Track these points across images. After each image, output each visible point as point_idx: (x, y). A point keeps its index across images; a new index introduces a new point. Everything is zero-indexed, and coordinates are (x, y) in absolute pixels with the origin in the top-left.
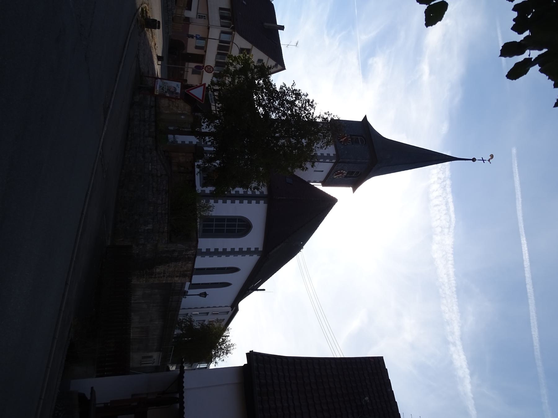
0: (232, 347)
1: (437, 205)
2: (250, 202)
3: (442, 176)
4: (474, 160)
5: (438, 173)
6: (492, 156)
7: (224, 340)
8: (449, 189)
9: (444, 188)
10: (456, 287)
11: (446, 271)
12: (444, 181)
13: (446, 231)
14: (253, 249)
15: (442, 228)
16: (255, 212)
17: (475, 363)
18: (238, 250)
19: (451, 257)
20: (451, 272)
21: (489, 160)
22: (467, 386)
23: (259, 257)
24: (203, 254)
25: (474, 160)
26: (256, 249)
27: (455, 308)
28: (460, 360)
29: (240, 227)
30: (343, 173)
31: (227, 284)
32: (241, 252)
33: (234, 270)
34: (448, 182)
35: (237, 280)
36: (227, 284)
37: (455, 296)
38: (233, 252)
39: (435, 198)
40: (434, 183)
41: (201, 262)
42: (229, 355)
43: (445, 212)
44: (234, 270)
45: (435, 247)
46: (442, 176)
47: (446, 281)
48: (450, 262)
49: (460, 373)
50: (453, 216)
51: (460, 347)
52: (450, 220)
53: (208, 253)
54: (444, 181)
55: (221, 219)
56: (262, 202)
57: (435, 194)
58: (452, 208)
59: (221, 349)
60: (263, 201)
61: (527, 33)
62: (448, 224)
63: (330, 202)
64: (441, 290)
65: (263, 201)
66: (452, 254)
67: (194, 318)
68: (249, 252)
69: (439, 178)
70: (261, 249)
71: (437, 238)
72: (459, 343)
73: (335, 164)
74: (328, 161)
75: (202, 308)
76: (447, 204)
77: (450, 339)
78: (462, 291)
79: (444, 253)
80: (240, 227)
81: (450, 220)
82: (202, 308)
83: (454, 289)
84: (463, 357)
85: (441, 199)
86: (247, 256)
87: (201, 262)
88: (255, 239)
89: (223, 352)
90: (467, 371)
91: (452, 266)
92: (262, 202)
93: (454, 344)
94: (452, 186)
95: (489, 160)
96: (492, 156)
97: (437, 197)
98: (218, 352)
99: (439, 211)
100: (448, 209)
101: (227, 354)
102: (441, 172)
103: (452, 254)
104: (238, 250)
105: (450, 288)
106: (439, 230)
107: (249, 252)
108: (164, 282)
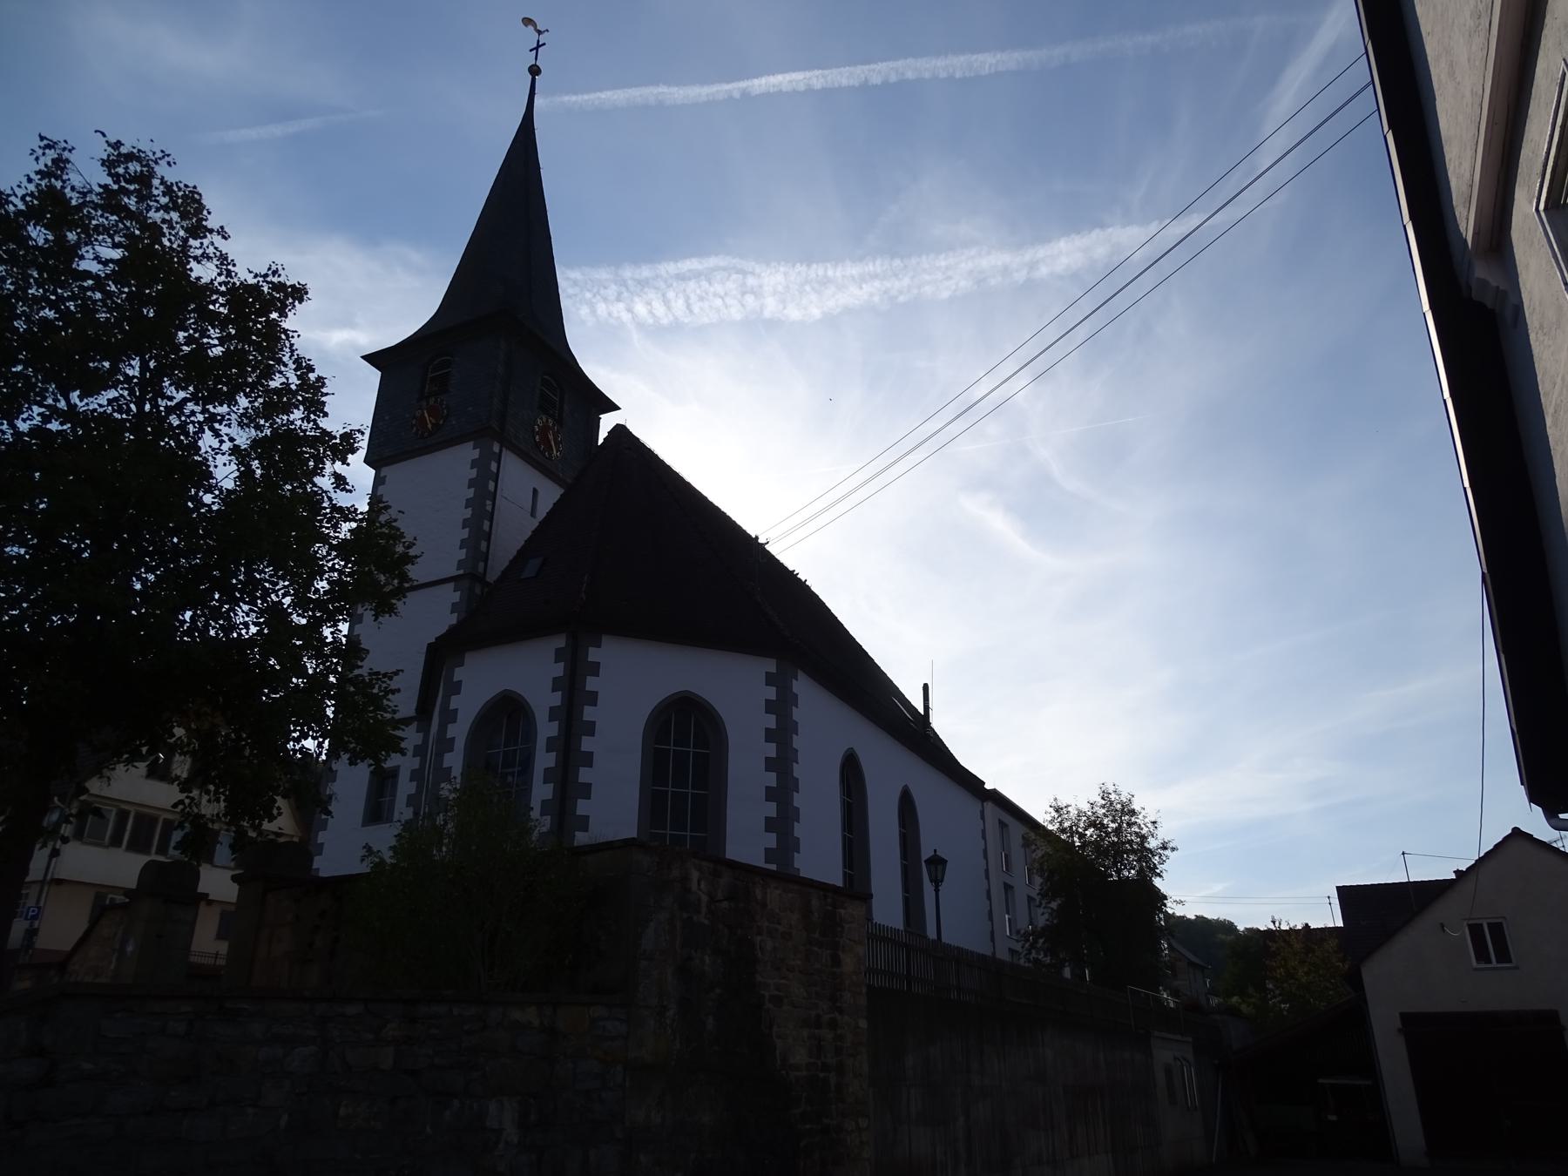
0: (1113, 797)
1: (689, 306)
2: (593, 698)
3: (612, 290)
4: (535, 71)
5: (605, 300)
6: (527, 21)
7: (1092, 824)
8: (645, 272)
9: (643, 284)
10: (892, 258)
11: (852, 285)
12: (624, 283)
13: (751, 281)
14: (771, 692)
15: (744, 294)
16: (633, 680)
17: (1076, 216)
18: (773, 717)
19: (817, 270)
20: (853, 270)
21: (540, 32)
22: (1126, 238)
23: (800, 674)
24: (787, 845)
25: (535, 71)
26: (770, 680)
27: (942, 262)
28: (1067, 254)
29: (684, 741)
30: (544, 430)
31: (907, 804)
32: (782, 734)
33: (851, 770)
34: (628, 273)
35: (888, 771)
36: (907, 804)
37: (914, 261)
38: (782, 763)
39: (669, 308)
40: (630, 310)
41: (820, 860)
42: (1136, 806)
43: (704, 284)
44: (851, 770)
45: (794, 314)
46: (612, 290)
47: (877, 284)
48: (830, 273)
49: (1101, 252)
50: (712, 262)
51: (1041, 252)
52: (724, 269)
53: (783, 823)
54: (624, 283)
55: (653, 804)
56: (593, 655)
57: (659, 309)
58: (691, 264)
59: (1118, 831)
60: (591, 650)
62: (734, 276)
63: (620, 431)
64: (901, 299)
65: (591, 650)
66: (809, 266)
67: (1024, 924)
68: (781, 707)
69: (618, 299)
70: (771, 666)
71: (771, 306)
72: (1028, 255)
73: (507, 444)
74: (494, 466)
75: (989, 897)
76: (681, 277)
77: (1020, 276)
78: (900, 243)
79: (808, 288)
80: (684, 741)
81: (724, 269)
82: (989, 897)
83: (897, 262)
84: (1062, 244)
85: (671, 294)
86: (797, 714)
87: (820, 860)
88: (735, 686)
89: (1130, 824)
90: (1096, 234)
91: (839, 269)
92: (593, 655)
93: (1033, 266)
94: (636, 261)
95: (540, 32)
96: (527, 21)
97: (666, 302)
98: (1130, 842)
99: (701, 299)
100: (697, 275)
101: (1133, 813)
102: (602, 291)
103: (809, 266)
104: (773, 717)
105: (896, 275)
106: (750, 299)
107: (781, 707)
108: (863, 1024)
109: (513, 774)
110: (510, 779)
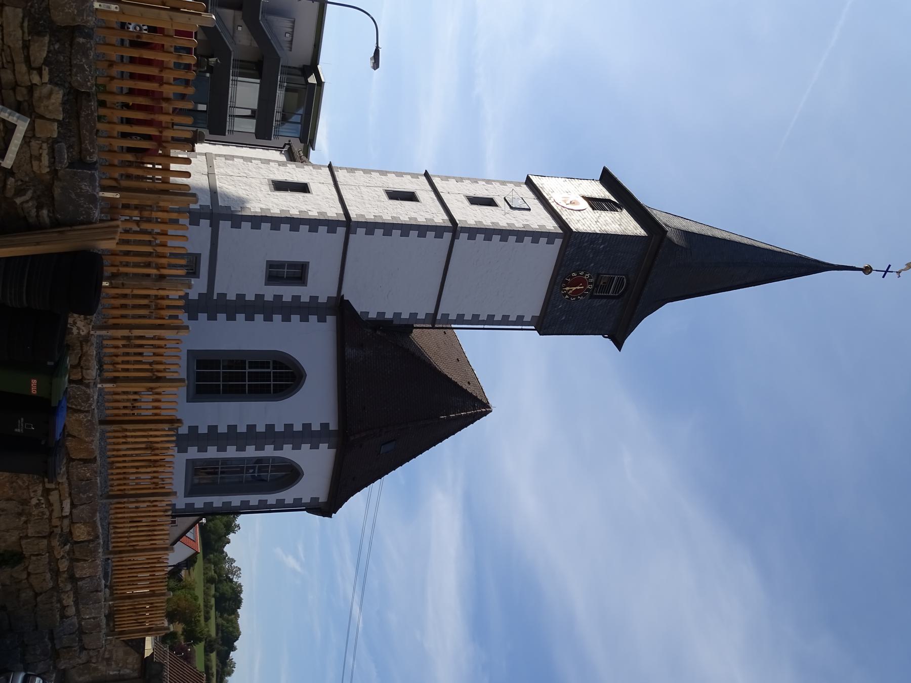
4: (867, 270)
25: (867, 270)
26: (325, 426)
61: (215, 298)
70: (333, 427)
92: (324, 446)
109: (254, 472)
110: (251, 471)
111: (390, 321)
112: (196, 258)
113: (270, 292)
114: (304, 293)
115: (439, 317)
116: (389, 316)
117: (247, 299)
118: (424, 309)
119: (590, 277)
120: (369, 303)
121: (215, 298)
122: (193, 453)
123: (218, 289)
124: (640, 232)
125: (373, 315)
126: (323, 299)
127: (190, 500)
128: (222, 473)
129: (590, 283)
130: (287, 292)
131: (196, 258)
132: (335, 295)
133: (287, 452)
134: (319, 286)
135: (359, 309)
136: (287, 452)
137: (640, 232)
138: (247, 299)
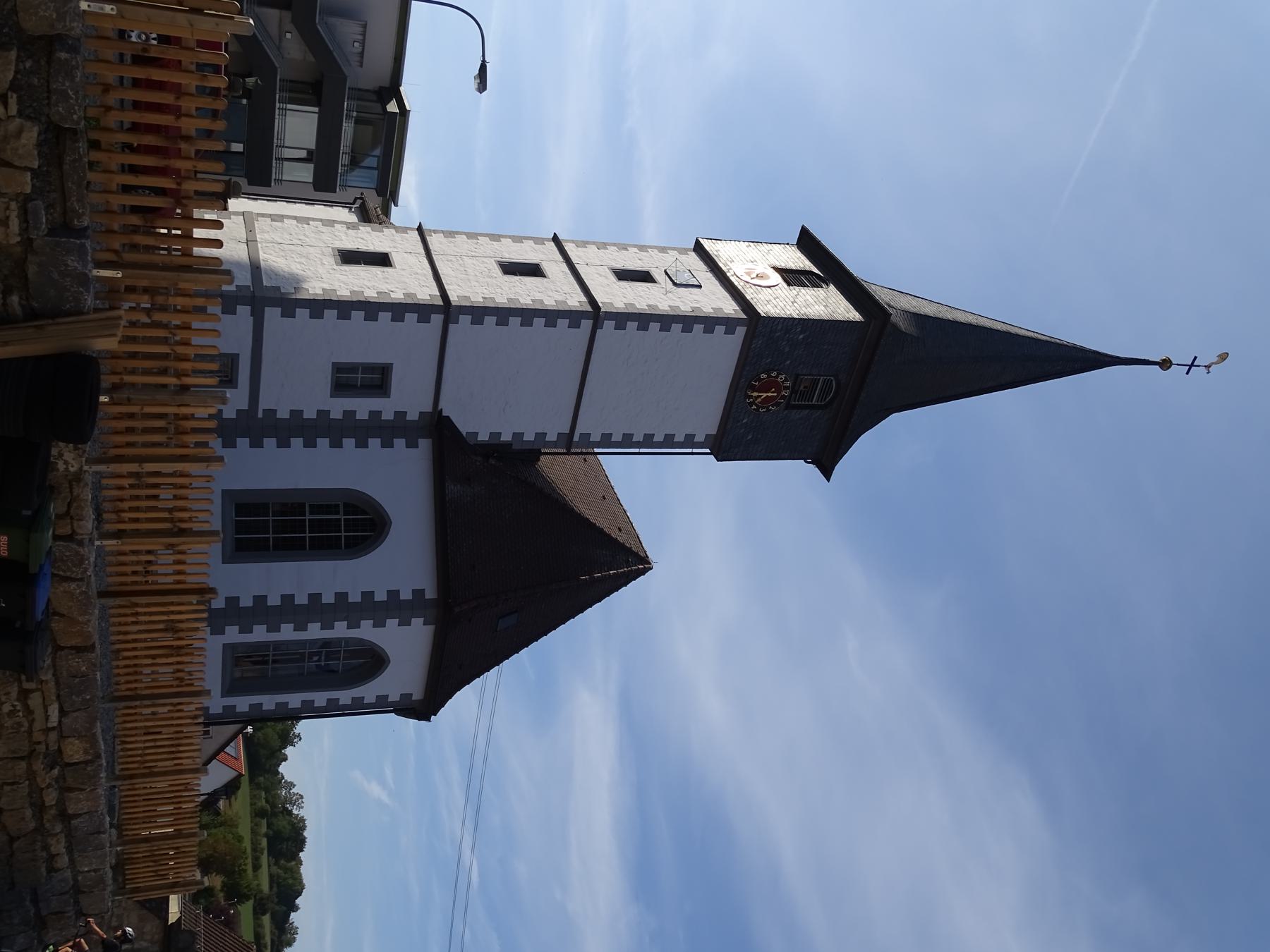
4: (1165, 364)
25: (1165, 364)
26: (418, 593)
56: (417, 622)
61: (260, 415)
70: (430, 594)
92: (417, 622)
95: (1208, 367)
109: (319, 660)
111: (508, 445)
112: (233, 359)
113: (338, 407)
114: (386, 407)
115: (576, 438)
116: (507, 437)
117: (379, 440)
118: (555, 427)
119: (786, 380)
120: (478, 419)
121: (260, 415)
122: (233, 634)
123: (264, 404)
124: (854, 315)
125: (483, 437)
126: (413, 416)
127: (230, 701)
128: (274, 662)
129: (786, 388)
130: (363, 407)
131: (233, 359)
132: (429, 409)
133: (366, 631)
134: (408, 397)
135: (464, 428)
136: (366, 631)
137: (854, 315)
138: (379, 440)
